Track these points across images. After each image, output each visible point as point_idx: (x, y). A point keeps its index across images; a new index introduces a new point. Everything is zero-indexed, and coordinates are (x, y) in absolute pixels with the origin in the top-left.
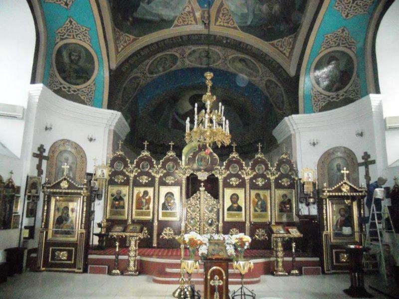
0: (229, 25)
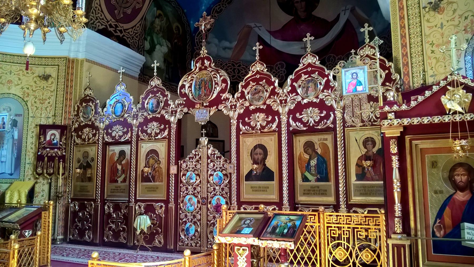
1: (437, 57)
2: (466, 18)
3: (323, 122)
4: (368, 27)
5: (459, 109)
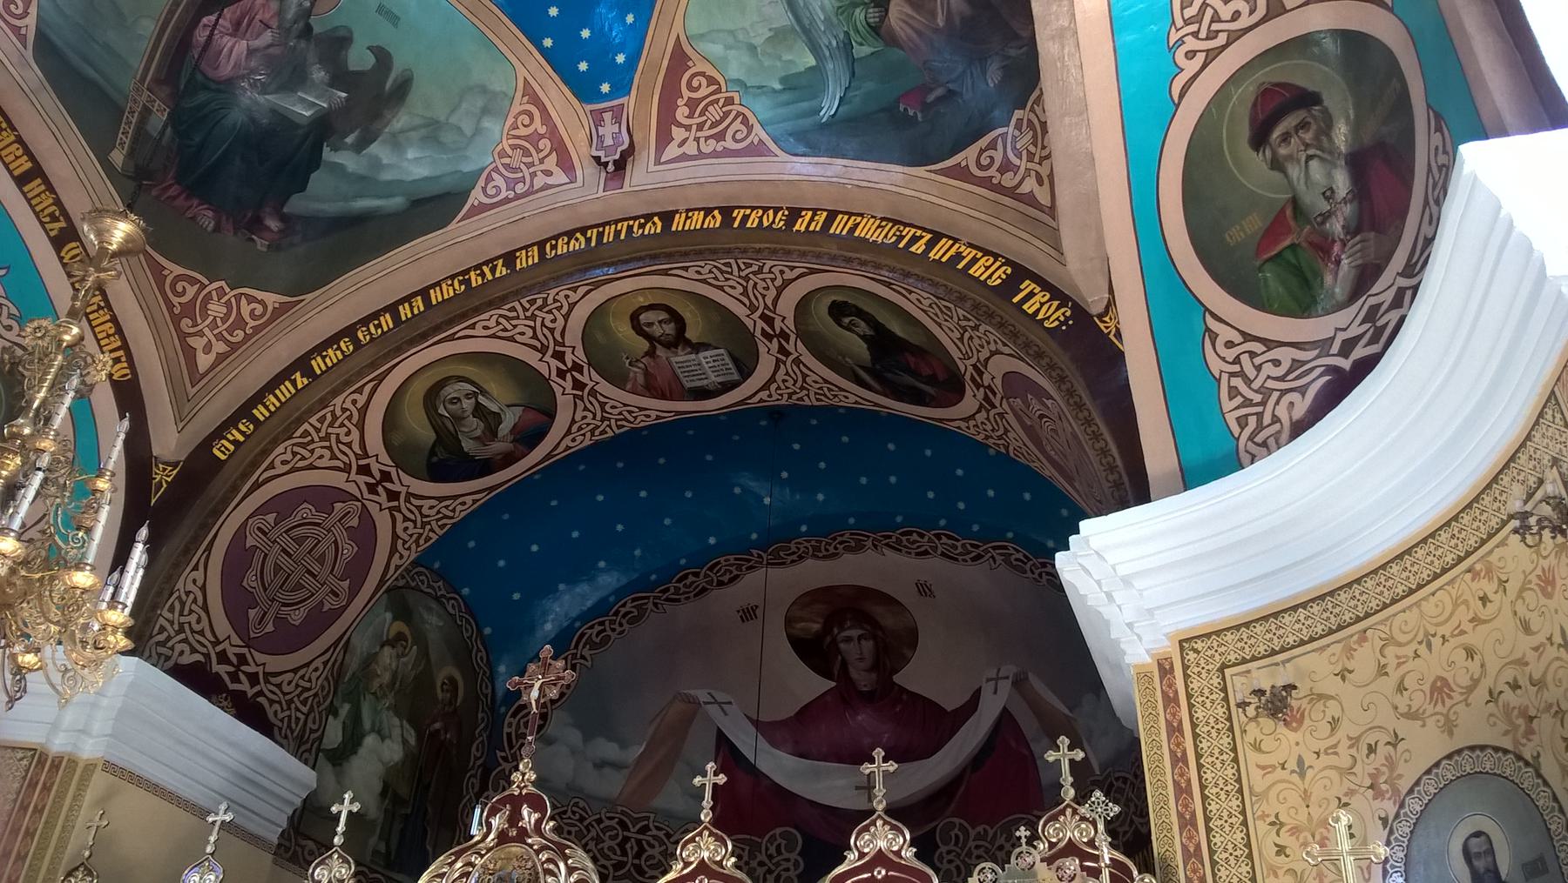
0: (729, 143)
1: (1298, 867)
2: (1372, 749)
4: (1071, 748)
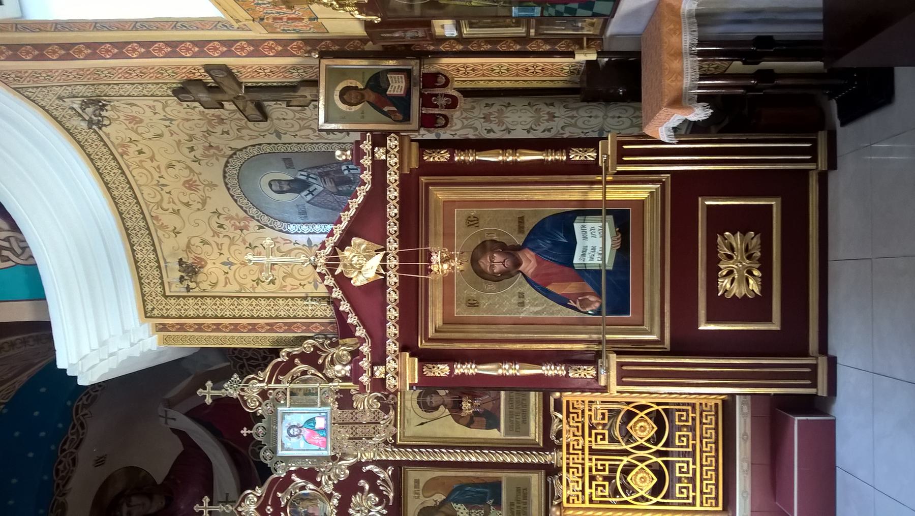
2: (221, 226)
3: (381, 488)
5: (377, 259)
